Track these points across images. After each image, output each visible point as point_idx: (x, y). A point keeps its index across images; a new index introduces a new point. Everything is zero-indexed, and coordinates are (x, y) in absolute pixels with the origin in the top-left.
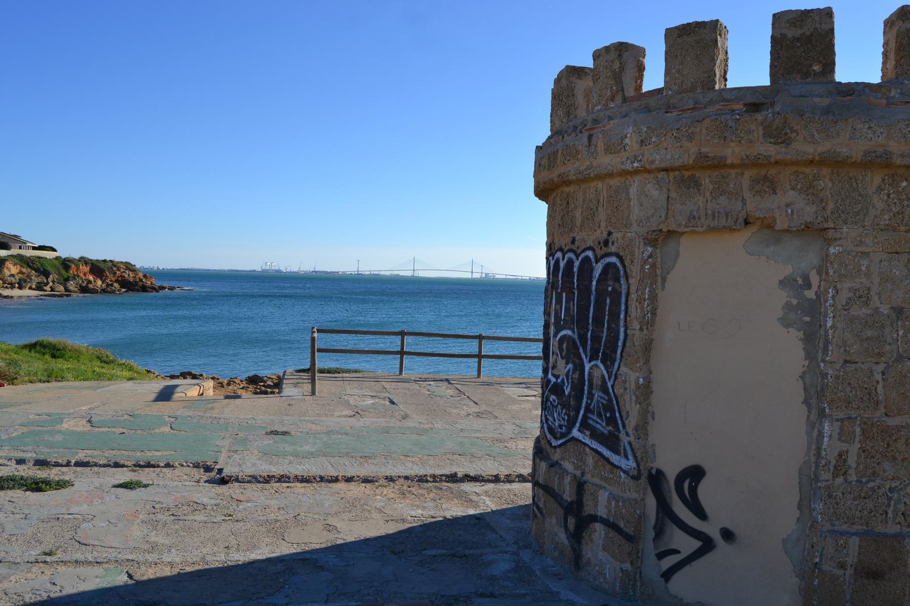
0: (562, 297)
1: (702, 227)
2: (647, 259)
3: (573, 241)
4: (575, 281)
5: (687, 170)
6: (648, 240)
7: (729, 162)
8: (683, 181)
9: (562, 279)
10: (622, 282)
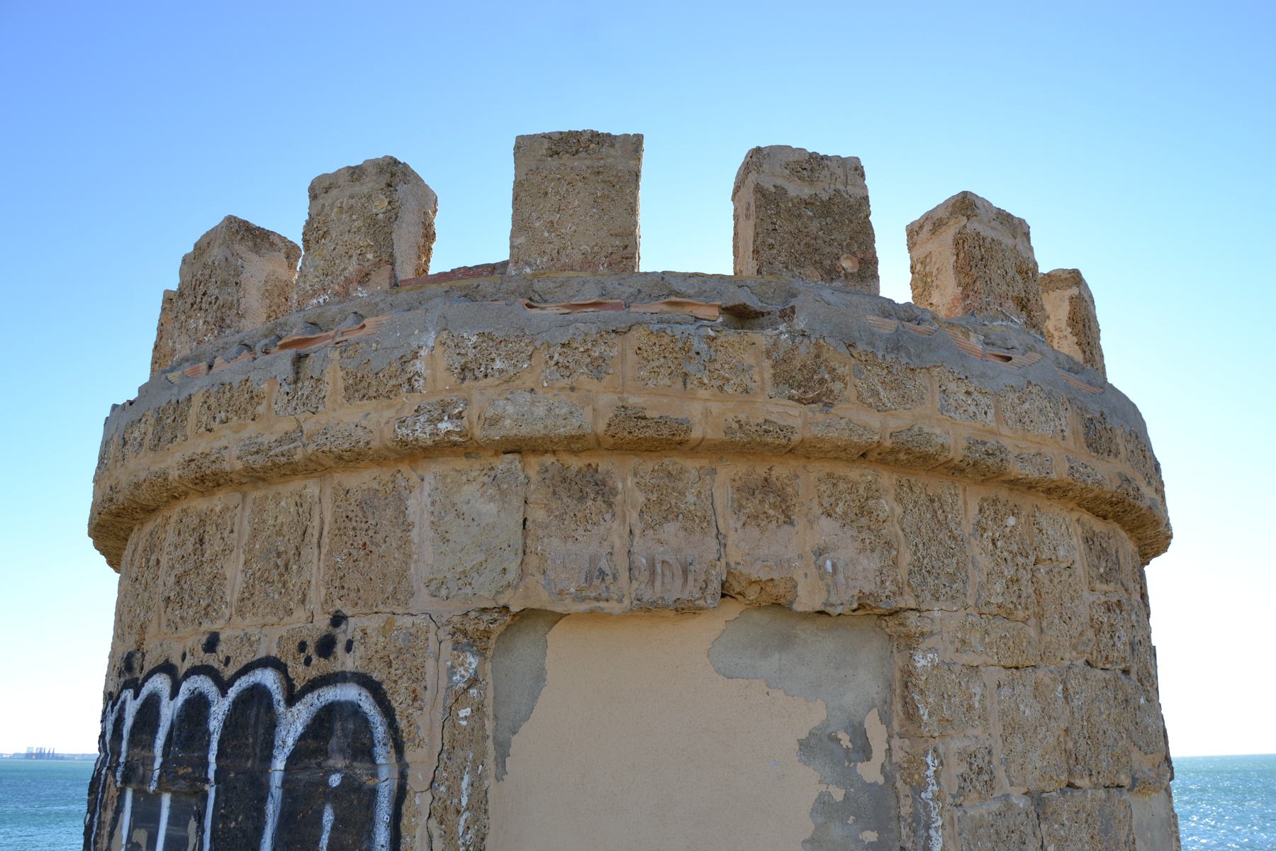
0: (159, 806)
1: (620, 601)
2: (466, 690)
3: (211, 644)
4: (212, 758)
5: (575, 453)
6: (465, 634)
7: (696, 434)
8: (564, 480)
9: (165, 754)
10: (380, 760)
